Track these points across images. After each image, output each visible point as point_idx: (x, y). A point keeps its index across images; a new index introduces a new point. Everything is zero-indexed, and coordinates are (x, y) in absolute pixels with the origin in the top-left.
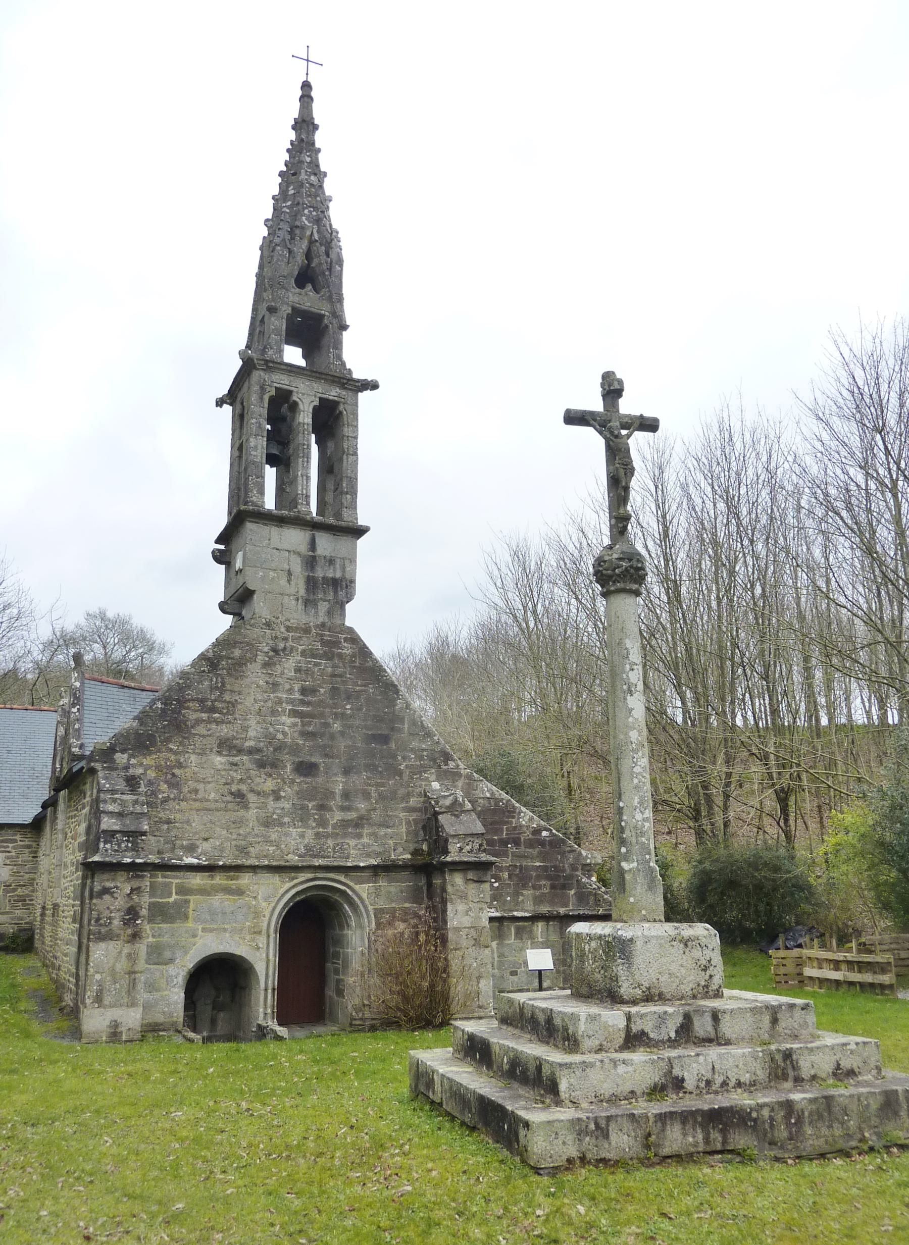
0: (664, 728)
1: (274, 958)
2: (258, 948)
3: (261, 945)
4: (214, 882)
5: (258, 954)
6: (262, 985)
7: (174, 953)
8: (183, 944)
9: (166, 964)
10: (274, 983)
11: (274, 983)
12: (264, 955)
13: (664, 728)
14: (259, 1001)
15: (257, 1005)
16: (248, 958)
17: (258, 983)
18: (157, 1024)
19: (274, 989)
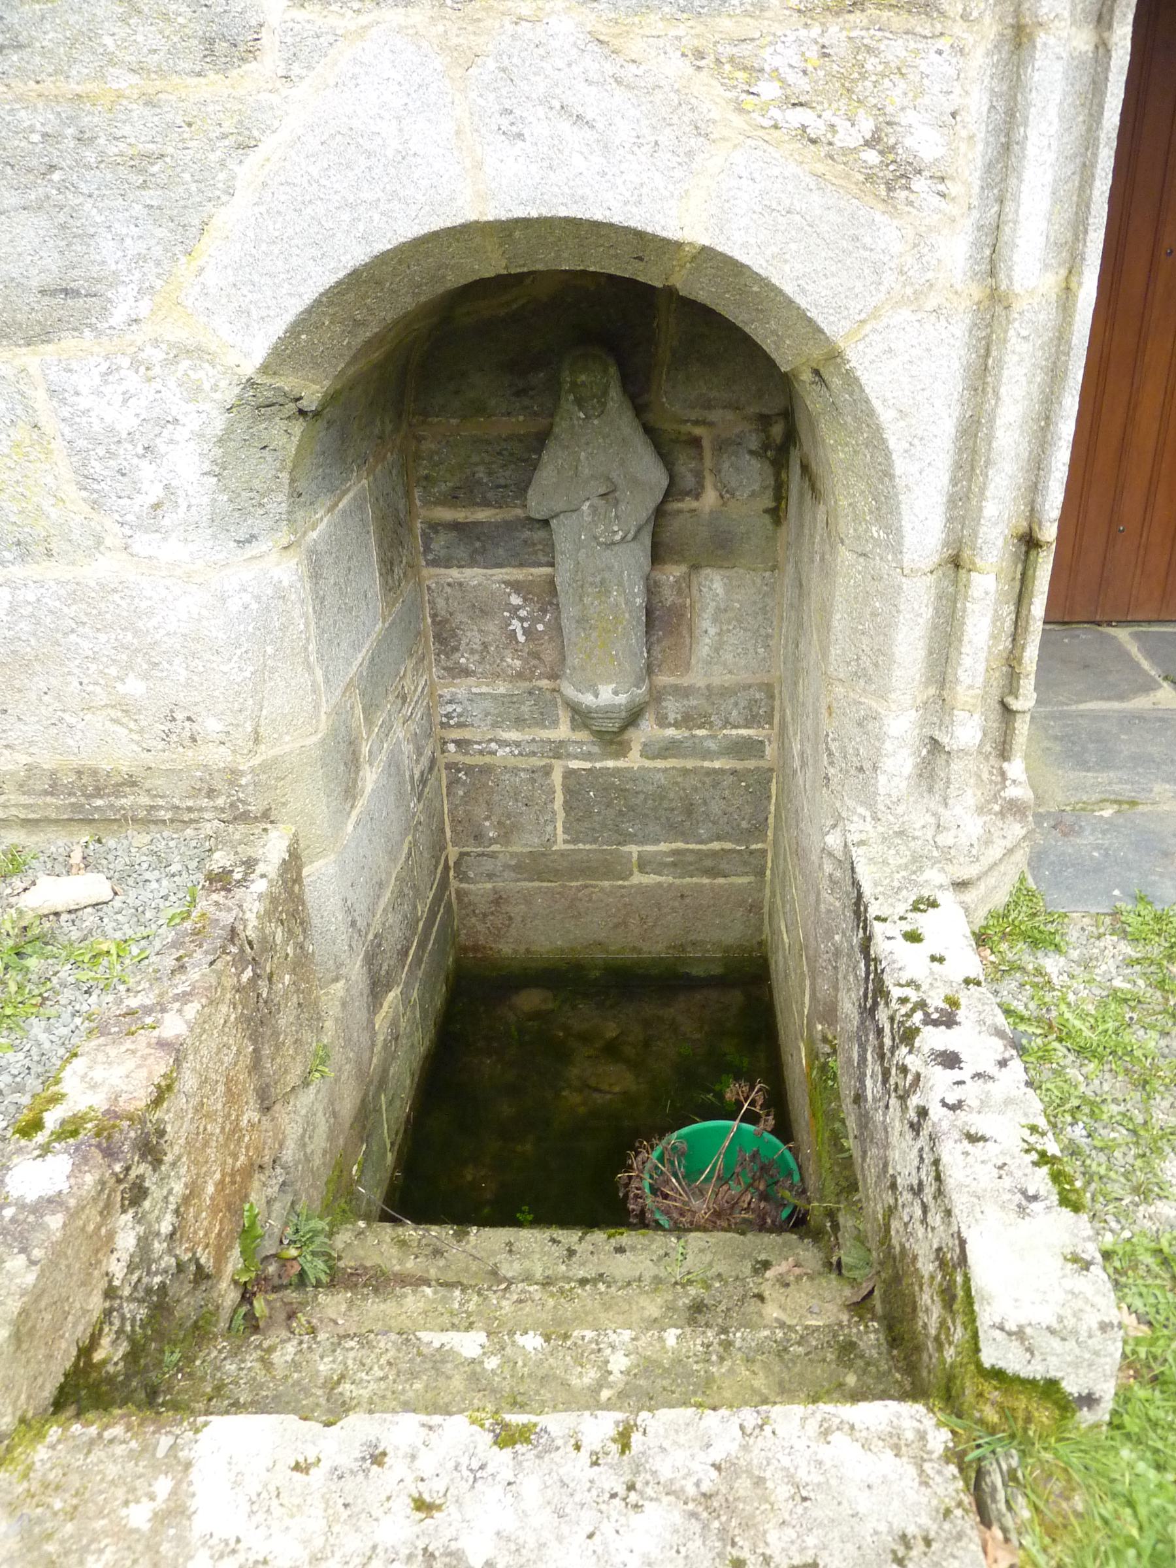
0: (278, 1496)
1: (1055, 274)
2: (894, 175)
3: (923, 141)
4: (621, 763)
5: (888, 233)
6: (923, 529)
7: (70, 233)
8: (138, 131)
9: (41, 335)
10: (1034, 489)
11: (1034, 489)
12: (955, 251)
13: (278, 1496)
14: (883, 655)
15: (872, 671)
16: (785, 277)
17: (885, 506)
18: (97, 784)
19: (1029, 542)
